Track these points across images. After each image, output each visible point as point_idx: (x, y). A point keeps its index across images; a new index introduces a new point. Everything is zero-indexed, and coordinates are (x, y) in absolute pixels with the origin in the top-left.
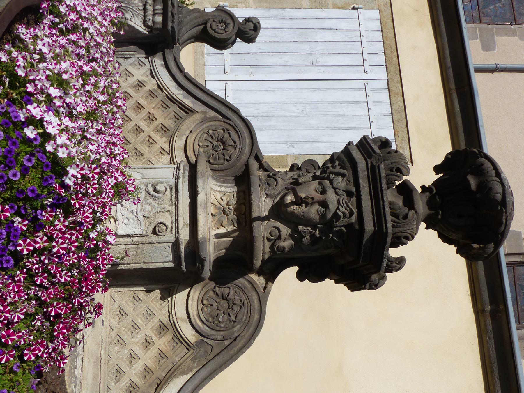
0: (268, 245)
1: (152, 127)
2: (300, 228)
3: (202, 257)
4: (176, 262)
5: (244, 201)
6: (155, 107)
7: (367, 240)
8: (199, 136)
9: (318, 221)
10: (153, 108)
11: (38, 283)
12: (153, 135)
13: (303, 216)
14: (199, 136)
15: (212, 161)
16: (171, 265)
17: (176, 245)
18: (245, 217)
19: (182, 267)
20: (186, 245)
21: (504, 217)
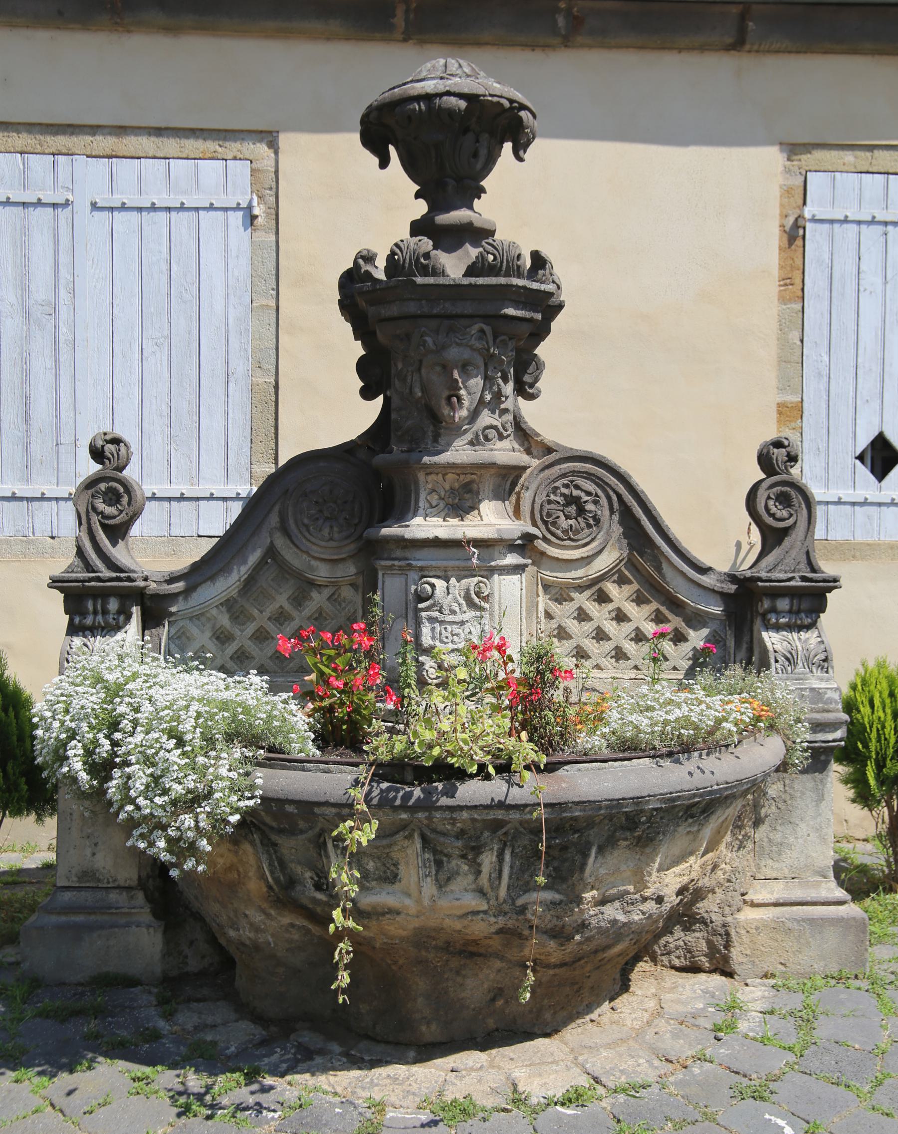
1: (295, 613)
5: (440, 475)
6: (258, 610)
8: (313, 540)
10: (261, 612)
11: (398, 802)
12: (307, 612)
14: (313, 540)
15: (356, 521)
18: (463, 474)
21: (490, 98)
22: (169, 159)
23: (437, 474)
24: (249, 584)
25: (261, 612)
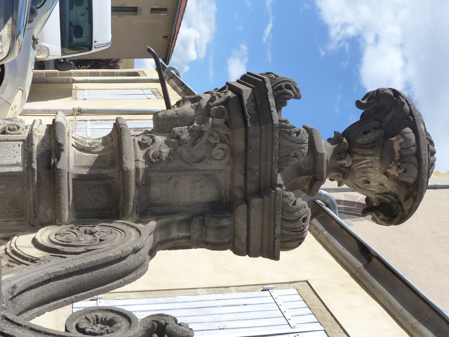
0: (141, 153)
2: (177, 129)
3: (60, 141)
4: (26, 165)
7: (248, 100)
9: (193, 114)
13: (177, 114)
16: (19, 169)
17: (28, 142)
19: (33, 164)
20: (40, 142)
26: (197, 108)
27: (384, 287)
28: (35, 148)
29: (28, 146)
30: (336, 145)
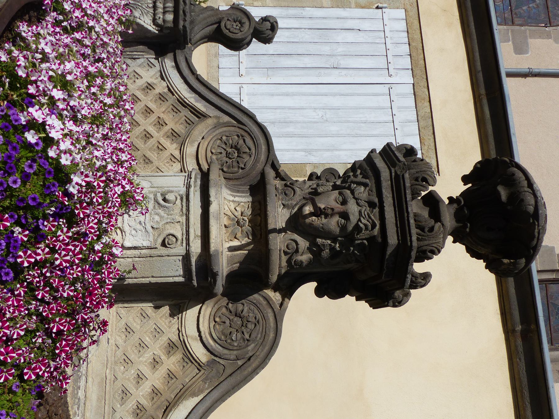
0: (284, 258)
1: (162, 133)
3: (215, 271)
5: (259, 212)
7: (391, 254)
8: (212, 142)
9: (338, 233)
10: (163, 113)
12: (163, 141)
13: (322, 228)
14: (212, 142)
15: (225, 169)
16: (181, 279)
17: (187, 257)
21: (536, 230)
22: (418, 122)
23: (260, 209)
24: (183, 103)
25: (163, 113)
26: (343, 228)
27: (476, 31)
28: (193, 263)
29: (187, 261)
30: (461, 225)
